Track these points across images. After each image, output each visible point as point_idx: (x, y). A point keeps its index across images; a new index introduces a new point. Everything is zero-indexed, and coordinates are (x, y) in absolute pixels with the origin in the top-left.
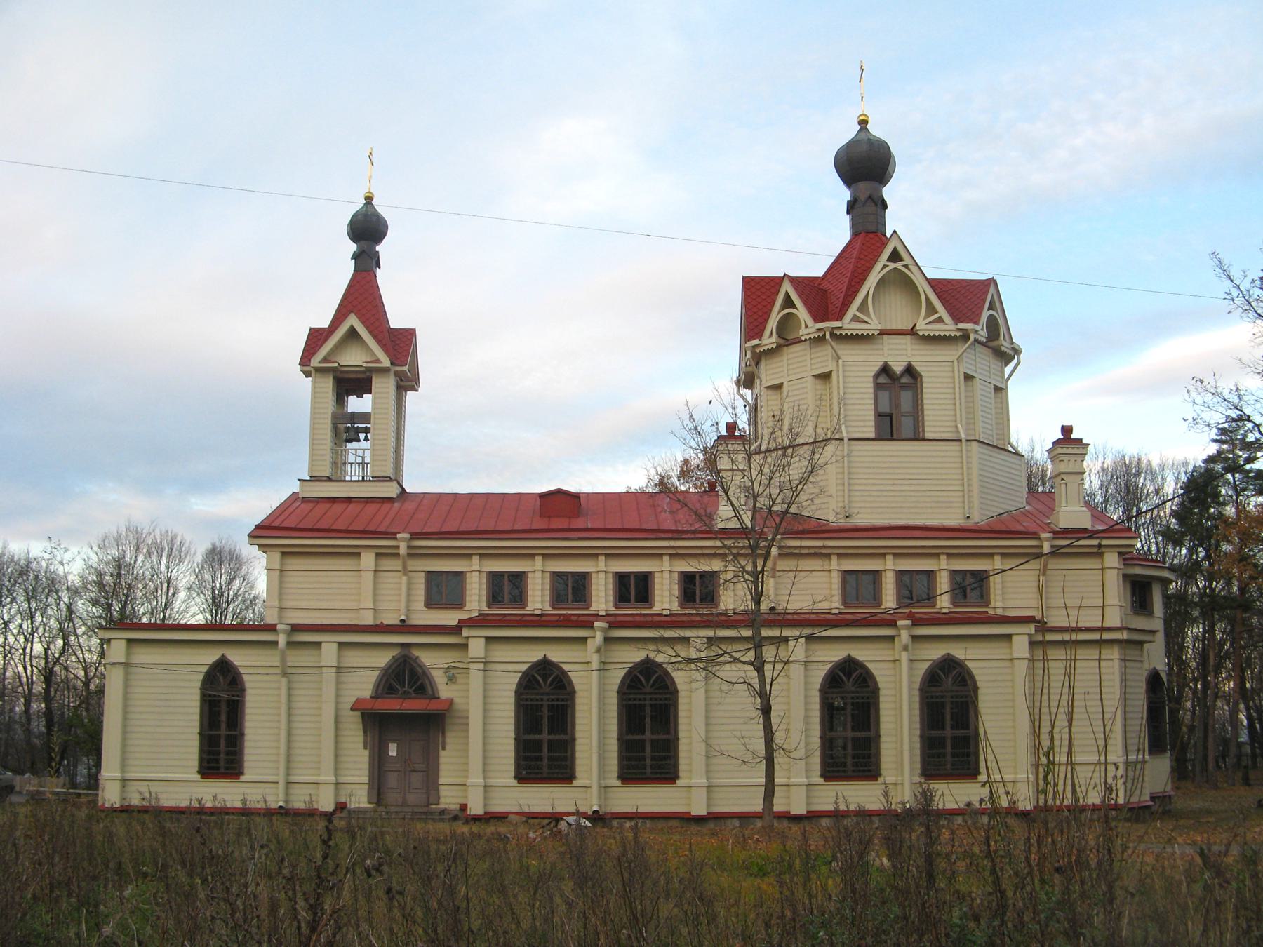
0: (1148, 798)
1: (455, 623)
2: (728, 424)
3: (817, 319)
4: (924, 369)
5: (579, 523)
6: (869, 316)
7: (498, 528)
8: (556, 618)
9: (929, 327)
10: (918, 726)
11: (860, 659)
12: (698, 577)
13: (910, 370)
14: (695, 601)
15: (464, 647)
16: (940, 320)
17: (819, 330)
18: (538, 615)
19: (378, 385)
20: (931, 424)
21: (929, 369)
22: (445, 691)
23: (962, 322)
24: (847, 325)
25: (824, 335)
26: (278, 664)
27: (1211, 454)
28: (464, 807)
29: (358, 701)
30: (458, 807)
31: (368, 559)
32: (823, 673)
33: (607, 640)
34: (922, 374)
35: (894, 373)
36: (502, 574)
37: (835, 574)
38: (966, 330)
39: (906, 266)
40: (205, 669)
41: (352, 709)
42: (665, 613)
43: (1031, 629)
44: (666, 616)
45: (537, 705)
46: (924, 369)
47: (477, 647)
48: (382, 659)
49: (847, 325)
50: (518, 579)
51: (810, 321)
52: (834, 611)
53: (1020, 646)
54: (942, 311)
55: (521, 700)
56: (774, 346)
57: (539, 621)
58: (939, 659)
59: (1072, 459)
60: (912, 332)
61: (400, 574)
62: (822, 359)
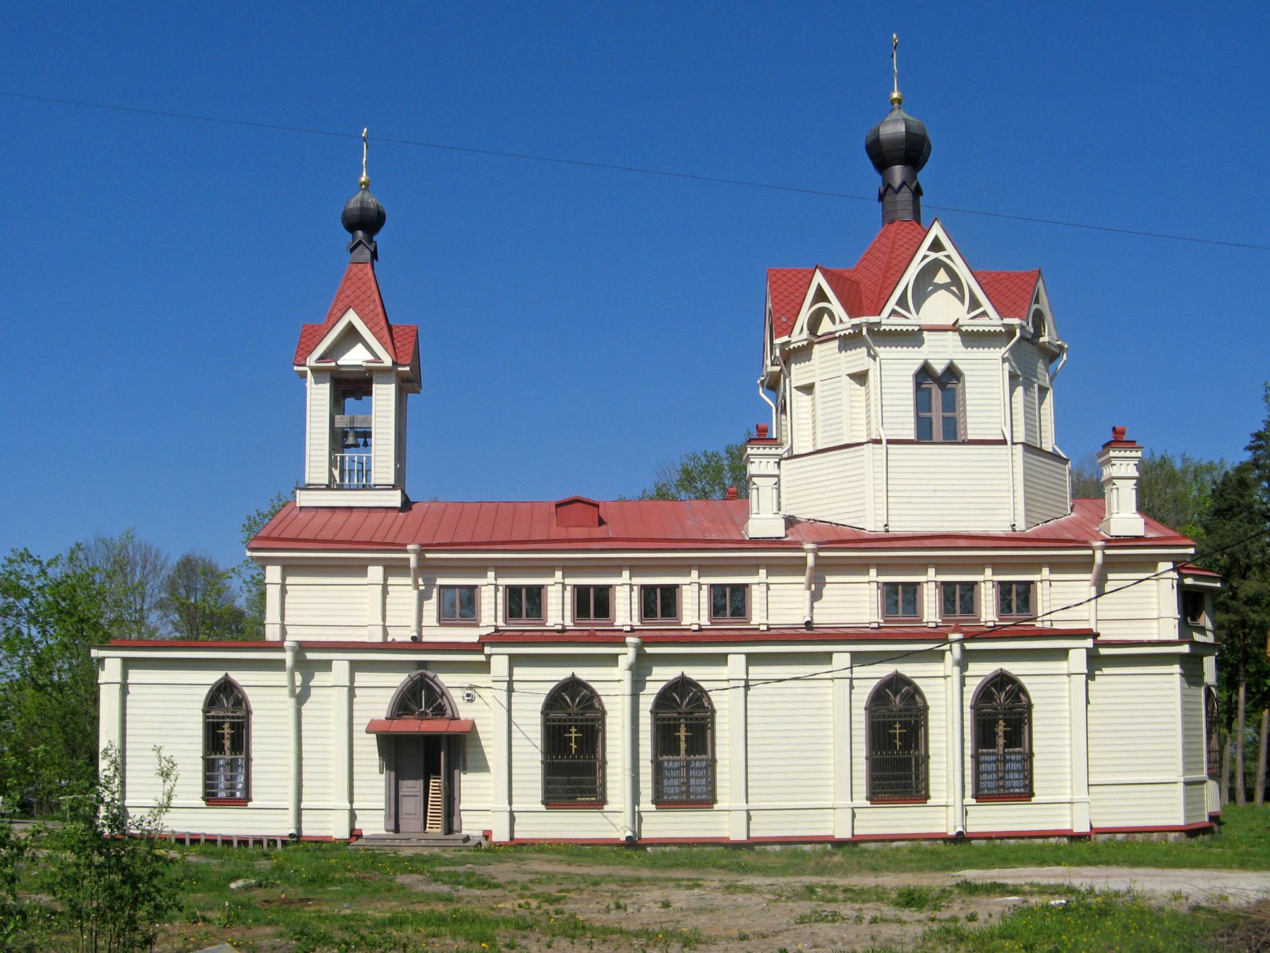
0: (1207, 819)
1: (476, 639)
3: (851, 315)
4: (966, 367)
5: (599, 532)
6: (908, 310)
7: (474, 540)
8: (586, 633)
11: (908, 675)
13: (952, 373)
14: (1011, 611)
15: (484, 667)
16: (984, 314)
17: (854, 326)
18: (558, 631)
21: (971, 367)
22: (465, 711)
23: (1006, 317)
25: (861, 331)
26: (285, 683)
27: (1244, 461)
28: (487, 835)
29: (373, 722)
30: (481, 834)
31: (376, 573)
32: (869, 690)
33: (964, 651)
35: (934, 372)
36: (587, 587)
38: (1012, 325)
39: (948, 257)
41: (367, 732)
43: (1089, 643)
44: (694, 631)
45: (565, 726)
46: (966, 367)
47: (500, 664)
49: (887, 321)
51: (845, 317)
52: (873, 625)
53: (1078, 660)
54: (986, 305)
55: (873, 717)
56: (805, 343)
57: (561, 636)
58: (674, 680)
60: (955, 327)
61: (411, 588)
62: (858, 359)
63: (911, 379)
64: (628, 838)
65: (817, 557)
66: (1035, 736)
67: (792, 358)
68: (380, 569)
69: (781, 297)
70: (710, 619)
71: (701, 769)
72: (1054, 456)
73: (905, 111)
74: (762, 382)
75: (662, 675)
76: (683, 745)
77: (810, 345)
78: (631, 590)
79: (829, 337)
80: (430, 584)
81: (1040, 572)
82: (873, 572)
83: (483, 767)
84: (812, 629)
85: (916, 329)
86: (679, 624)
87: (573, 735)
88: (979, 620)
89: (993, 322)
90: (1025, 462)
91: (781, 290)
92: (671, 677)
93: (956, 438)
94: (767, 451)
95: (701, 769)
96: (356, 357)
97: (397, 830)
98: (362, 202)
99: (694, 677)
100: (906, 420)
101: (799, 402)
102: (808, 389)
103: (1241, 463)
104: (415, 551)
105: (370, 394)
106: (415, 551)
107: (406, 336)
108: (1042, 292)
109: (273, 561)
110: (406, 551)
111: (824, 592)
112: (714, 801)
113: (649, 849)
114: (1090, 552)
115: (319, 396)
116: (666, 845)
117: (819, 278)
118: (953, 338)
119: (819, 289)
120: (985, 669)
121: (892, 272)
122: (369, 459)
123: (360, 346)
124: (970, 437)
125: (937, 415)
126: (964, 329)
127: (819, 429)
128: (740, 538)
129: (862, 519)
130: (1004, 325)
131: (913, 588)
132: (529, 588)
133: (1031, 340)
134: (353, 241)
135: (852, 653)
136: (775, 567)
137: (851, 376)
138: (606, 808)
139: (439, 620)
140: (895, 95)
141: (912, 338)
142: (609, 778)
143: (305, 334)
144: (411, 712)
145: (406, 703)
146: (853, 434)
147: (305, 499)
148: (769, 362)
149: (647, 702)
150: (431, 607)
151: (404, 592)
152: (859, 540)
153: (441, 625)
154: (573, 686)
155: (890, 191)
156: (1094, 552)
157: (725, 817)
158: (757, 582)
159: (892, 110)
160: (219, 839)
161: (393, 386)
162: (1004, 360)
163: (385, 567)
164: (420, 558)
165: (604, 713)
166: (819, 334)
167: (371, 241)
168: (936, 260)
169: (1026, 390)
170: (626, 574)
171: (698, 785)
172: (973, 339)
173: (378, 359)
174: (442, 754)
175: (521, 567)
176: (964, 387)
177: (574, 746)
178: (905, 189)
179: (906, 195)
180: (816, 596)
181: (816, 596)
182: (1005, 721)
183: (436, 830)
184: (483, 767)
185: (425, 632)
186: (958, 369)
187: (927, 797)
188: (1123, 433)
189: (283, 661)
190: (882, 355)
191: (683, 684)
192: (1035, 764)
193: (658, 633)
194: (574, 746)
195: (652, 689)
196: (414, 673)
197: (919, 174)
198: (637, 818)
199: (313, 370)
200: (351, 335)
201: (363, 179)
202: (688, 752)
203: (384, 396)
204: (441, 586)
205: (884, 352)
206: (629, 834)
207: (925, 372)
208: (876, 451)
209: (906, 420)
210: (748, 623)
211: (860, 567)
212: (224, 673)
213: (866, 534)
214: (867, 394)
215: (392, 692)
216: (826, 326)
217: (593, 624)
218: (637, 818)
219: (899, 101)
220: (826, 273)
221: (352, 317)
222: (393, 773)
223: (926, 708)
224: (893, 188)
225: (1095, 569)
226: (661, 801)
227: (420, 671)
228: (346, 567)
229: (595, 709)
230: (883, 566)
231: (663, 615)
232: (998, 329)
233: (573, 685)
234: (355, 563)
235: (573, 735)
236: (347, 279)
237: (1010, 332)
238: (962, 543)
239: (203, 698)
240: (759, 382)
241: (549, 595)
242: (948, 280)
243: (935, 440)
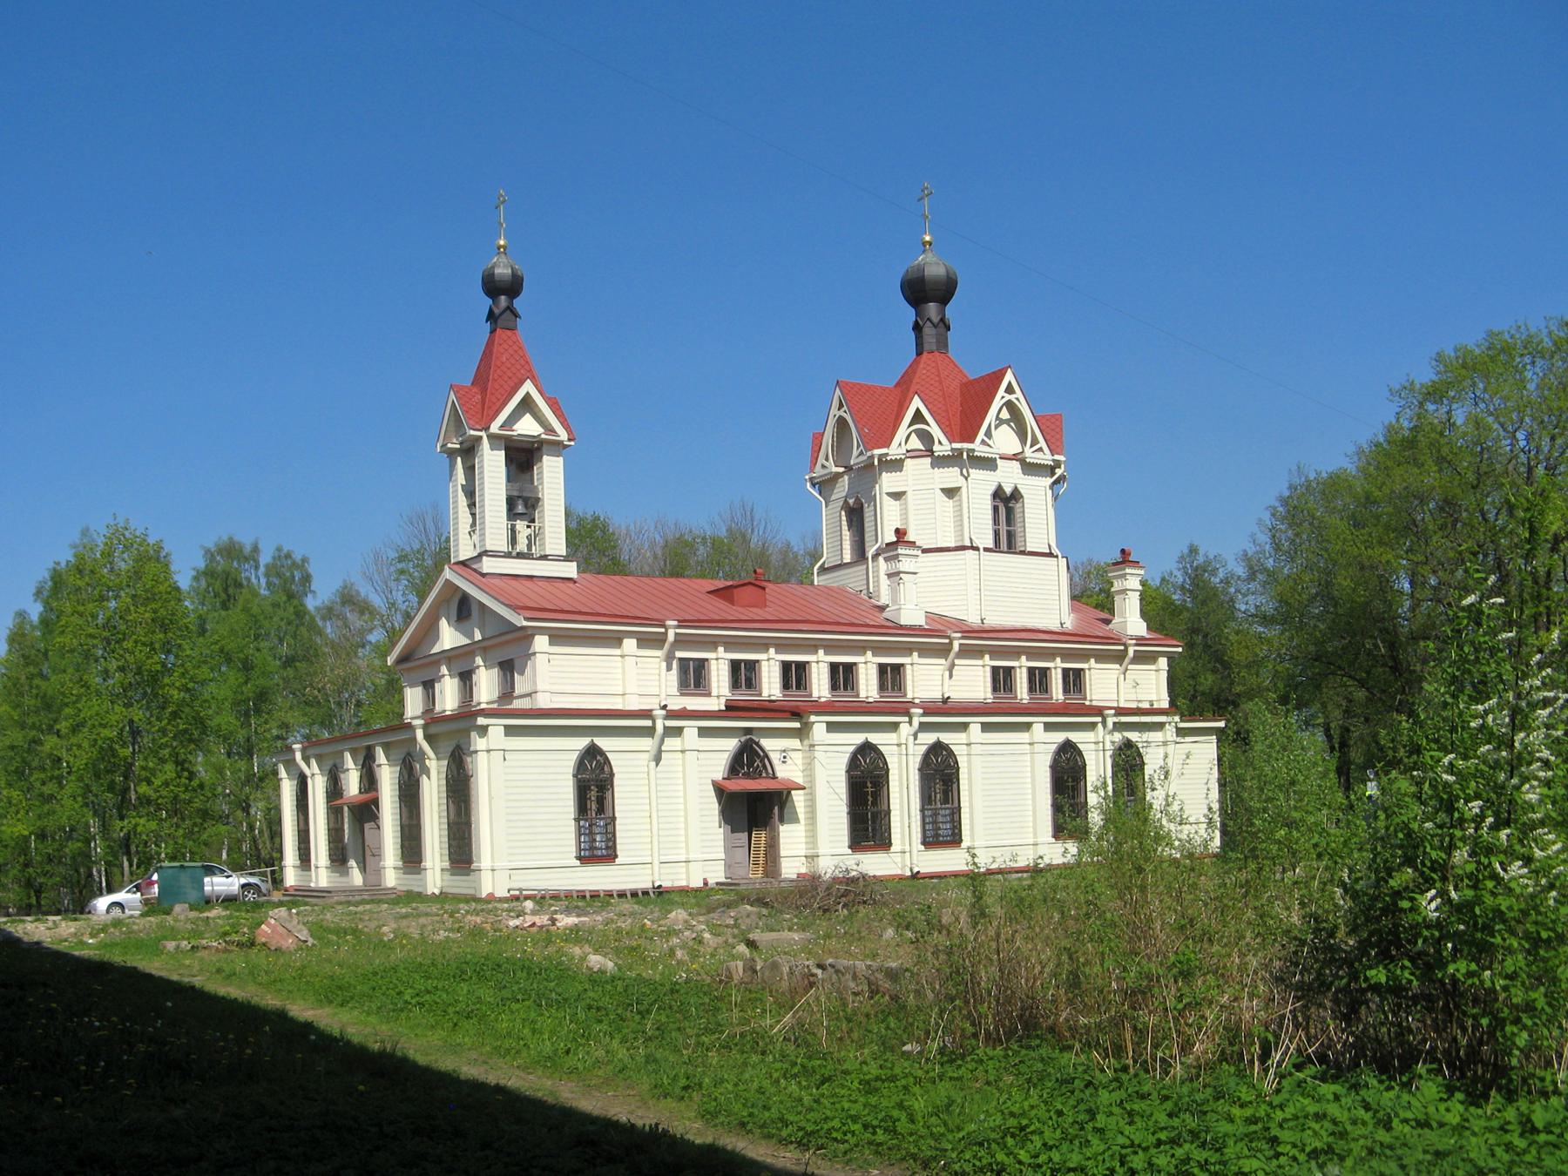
12: (1001, 671)
13: (1016, 495)
16: (1040, 449)
20: (987, 531)
22: (783, 772)
25: (962, 454)
34: (1025, 496)
35: (1005, 492)
36: (740, 661)
39: (1017, 399)
40: (852, 749)
48: (732, 744)
49: (977, 447)
54: (1042, 443)
62: (951, 476)
66: (616, 801)
81: (816, 652)
83: (796, 820)
88: (811, 696)
89: (1046, 458)
96: (527, 427)
102: (897, 496)
109: (542, 631)
114: (663, 630)
115: (493, 463)
116: (932, 877)
117: (917, 403)
118: (1016, 465)
119: (918, 411)
120: (929, 738)
124: (1028, 549)
126: (1028, 460)
130: (1053, 460)
132: (747, 662)
135: (827, 723)
136: (926, 651)
137: (943, 490)
141: (988, 464)
153: (682, 694)
156: (666, 631)
160: (562, 895)
161: (503, 452)
172: (1030, 468)
175: (579, 637)
182: (597, 787)
184: (796, 820)
186: (1020, 493)
187: (890, 844)
188: (905, 533)
190: (972, 476)
192: (617, 827)
193: (842, 704)
196: (743, 739)
204: (680, 659)
212: (590, 739)
215: (848, 755)
221: (528, 387)
225: (667, 646)
227: (748, 737)
228: (579, 637)
230: (996, 653)
231: (893, 689)
235: (870, 790)
238: (1023, 635)
239: (572, 763)
240: (807, 477)
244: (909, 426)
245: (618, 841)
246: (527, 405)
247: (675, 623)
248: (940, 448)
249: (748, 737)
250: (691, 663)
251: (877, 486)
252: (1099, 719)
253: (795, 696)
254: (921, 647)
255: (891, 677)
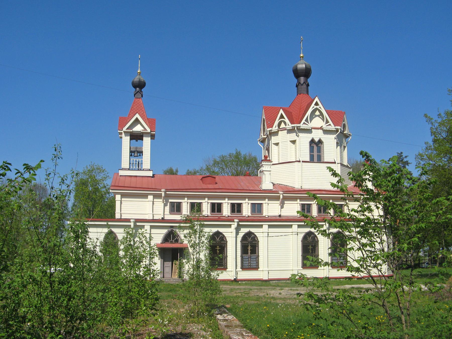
2: (407, 161)
3: (292, 123)
5: (216, 186)
9: (327, 127)
10: (301, 252)
12: (216, 204)
13: (320, 142)
16: (330, 125)
17: (292, 127)
18: (206, 216)
19: (145, 140)
20: (326, 156)
24: (302, 125)
31: (150, 198)
35: (315, 141)
37: (299, 204)
39: (320, 107)
42: (226, 216)
48: (165, 231)
49: (302, 125)
50: (220, 205)
51: (290, 124)
54: (331, 122)
56: (277, 131)
59: (267, 166)
60: (321, 128)
62: (293, 136)
63: (308, 143)
64: (235, 279)
65: (283, 196)
67: (272, 135)
68: (120, 196)
69: (268, 115)
70: (251, 213)
71: (254, 258)
72: (347, 166)
73: (304, 60)
74: (259, 140)
75: (244, 231)
76: (249, 252)
77: (278, 131)
78: (188, 204)
79: (284, 129)
80: (167, 202)
82: (298, 200)
84: (281, 217)
85: (311, 128)
86: (242, 215)
87: (218, 248)
90: (341, 169)
91: (268, 113)
92: (246, 231)
93: (320, 161)
94: (268, 164)
95: (254, 258)
96: (138, 128)
97: (164, 277)
98: (139, 79)
99: (253, 231)
100: (307, 155)
101: (274, 149)
102: (277, 144)
103: (137, 141)
104: (164, 191)
105: (142, 140)
106: (164, 191)
107: (152, 122)
108: (345, 118)
109: (118, 193)
110: (161, 191)
111: (284, 206)
112: (259, 268)
113: (240, 282)
115: (126, 140)
117: (281, 112)
118: (321, 131)
121: (302, 110)
122: (142, 161)
123: (139, 125)
124: (325, 161)
125: (315, 154)
126: (324, 129)
127: (280, 157)
128: (259, 189)
129: (294, 184)
130: (335, 128)
131: (309, 205)
133: (342, 133)
134: (136, 91)
135: (298, 225)
136: (270, 198)
137: (291, 141)
138: (227, 270)
139: (170, 213)
140: (302, 55)
141: (309, 131)
142: (228, 261)
143: (120, 120)
144: (168, 241)
145: (167, 239)
146: (291, 158)
147: (121, 173)
148: (262, 135)
149: (239, 239)
150: (168, 208)
151: (159, 203)
152: (294, 191)
153: (170, 214)
154: (218, 234)
155: (300, 84)
157: (261, 273)
158: (265, 202)
159: (301, 60)
161: (129, 137)
162: (335, 138)
163: (121, 195)
164: (165, 194)
165: (227, 242)
166: (280, 128)
167: (141, 91)
168: (317, 108)
169: (340, 147)
170: (186, 199)
171: (253, 264)
172: (326, 132)
173: (145, 129)
174: (179, 254)
175: (128, 195)
176: (323, 146)
177: (218, 252)
178: (304, 84)
179: (305, 86)
180: (282, 207)
181: (282, 207)
183: (176, 277)
185: (165, 216)
189: (130, 225)
190: (300, 136)
191: (250, 233)
194: (218, 252)
195: (241, 235)
196: (170, 230)
197: (308, 80)
198: (237, 273)
199: (124, 132)
200: (137, 122)
201: (139, 71)
202: (251, 253)
203: (147, 141)
204: (170, 202)
205: (301, 135)
206: (235, 278)
207: (312, 141)
208: (299, 164)
209: (307, 155)
210: (262, 215)
211: (295, 199)
213: (296, 189)
214: (296, 147)
216: (283, 125)
217: (216, 215)
218: (237, 273)
219: (303, 57)
220: (283, 110)
221: (137, 116)
222: (163, 260)
223: (318, 241)
224: (301, 84)
225: (280, 200)
226: (243, 268)
227: (171, 229)
228: (128, 195)
229: (224, 240)
230: (301, 199)
231: (258, 212)
232: (334, 129)
233: (218, 233)
234: (287, 197)
236: (134, 103)
237: (337, 130)
238: (324, 192)
241: (203, 205)
242: (319, 114)
243: (315, 161)
244: (279, 119)
245: (260, 263)
246: (137, 121)
247: (282, 193)
248: (288, 126)
249: (171, 229)
250: (175, 203)
251: (270, 141)
252: (324, 223)
253: (257, 215)
254: (249, 197)
255: (256, 208)
